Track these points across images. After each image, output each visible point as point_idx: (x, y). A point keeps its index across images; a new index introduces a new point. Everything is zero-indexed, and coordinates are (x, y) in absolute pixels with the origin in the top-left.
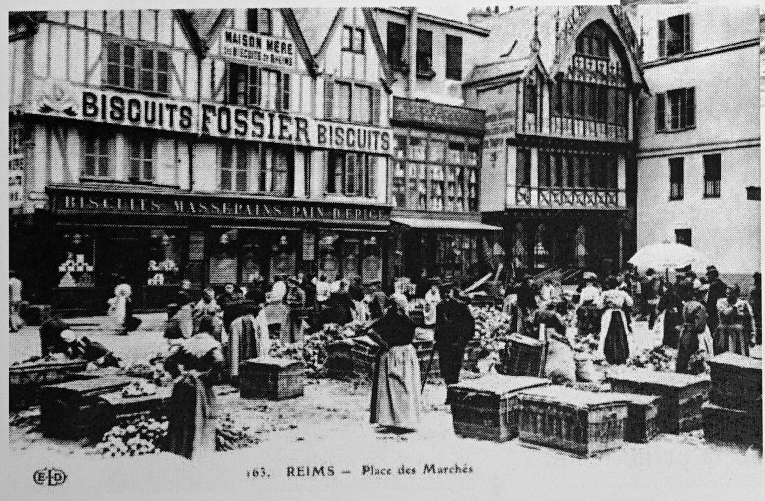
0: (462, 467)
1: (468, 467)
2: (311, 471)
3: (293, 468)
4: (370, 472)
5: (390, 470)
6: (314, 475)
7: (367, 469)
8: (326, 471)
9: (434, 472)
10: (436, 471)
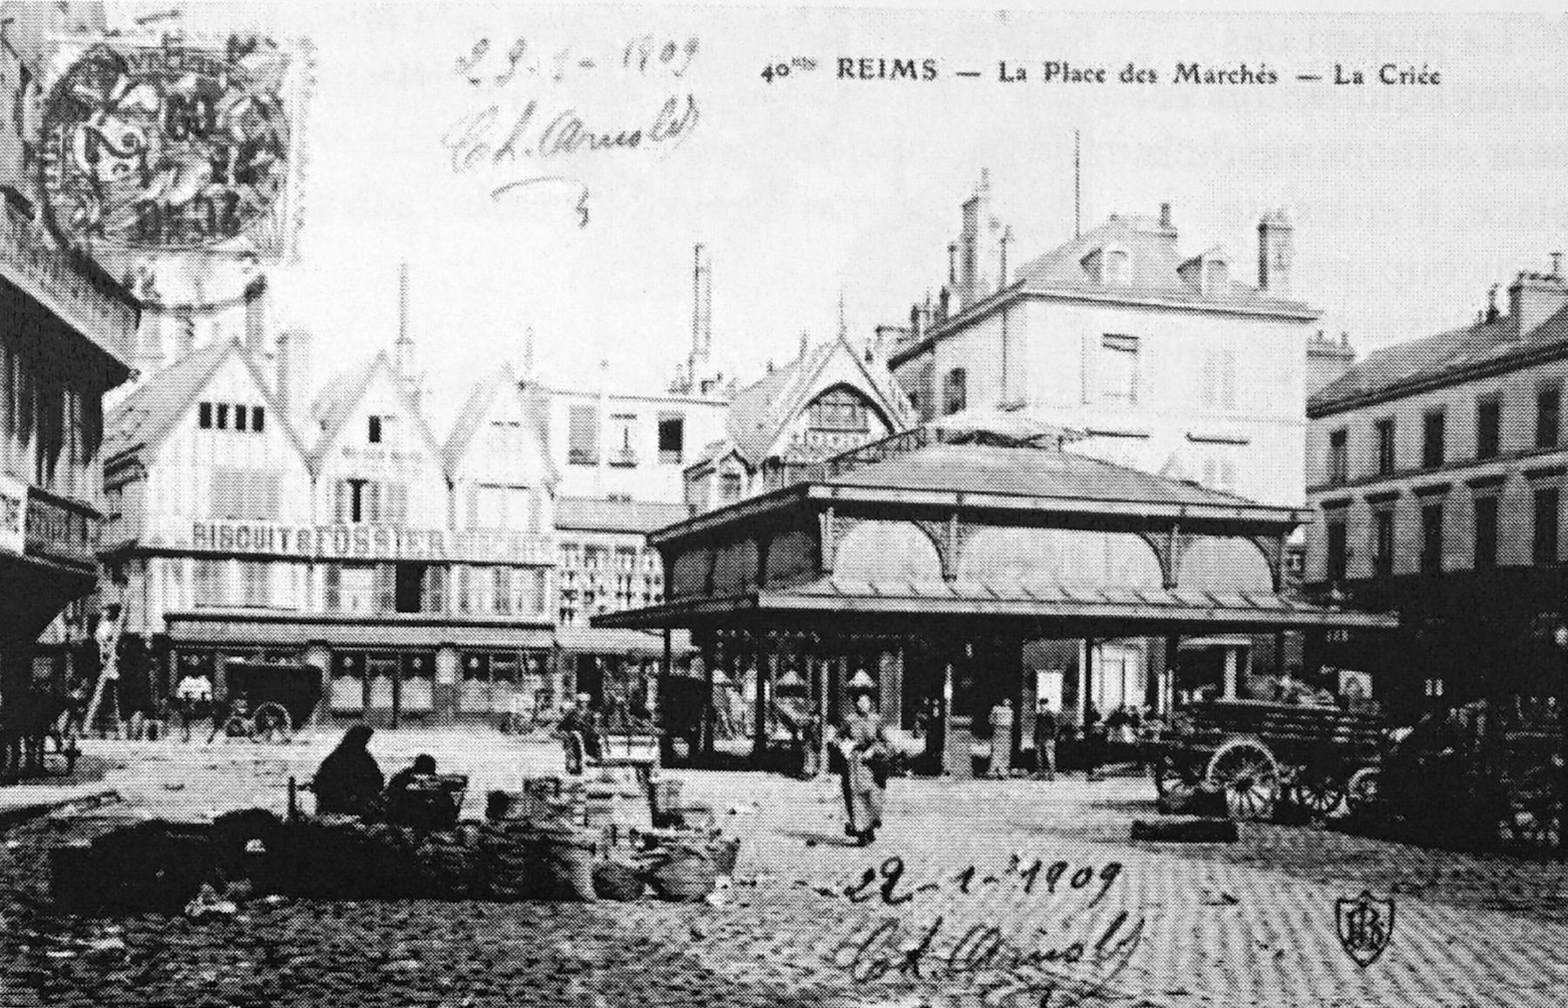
0: (1255, 71)
1: (1430, 71)
2: (889, 67)
3: (851, 62)
4: (1061, 76)
5: (1437, 74)
6: (893, 75)
7: (1053, 68)
8: (919, 69)
9: (1197, 80)
10: (1202, 77)
